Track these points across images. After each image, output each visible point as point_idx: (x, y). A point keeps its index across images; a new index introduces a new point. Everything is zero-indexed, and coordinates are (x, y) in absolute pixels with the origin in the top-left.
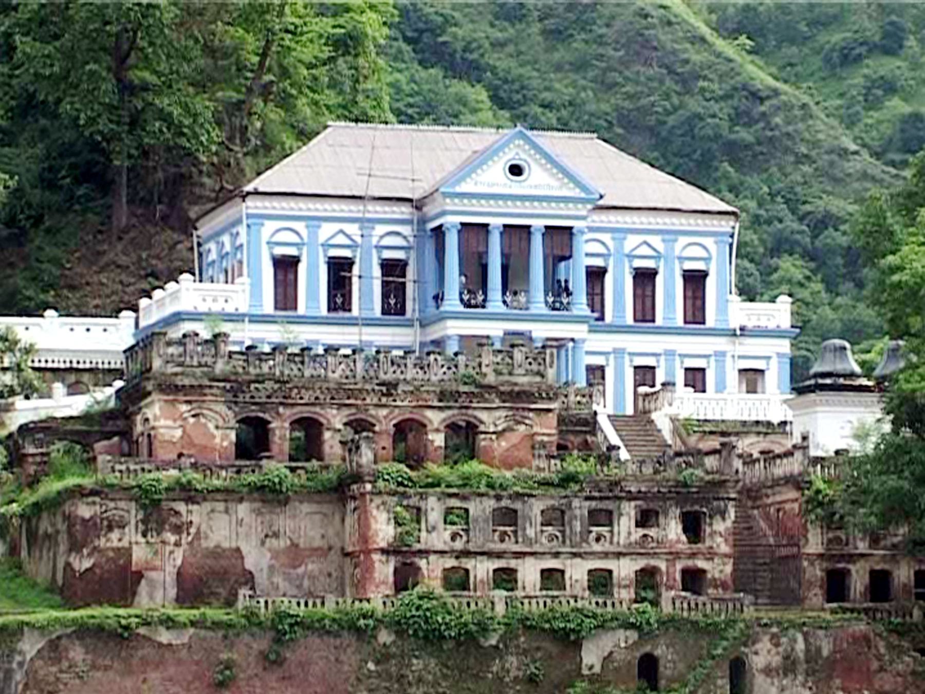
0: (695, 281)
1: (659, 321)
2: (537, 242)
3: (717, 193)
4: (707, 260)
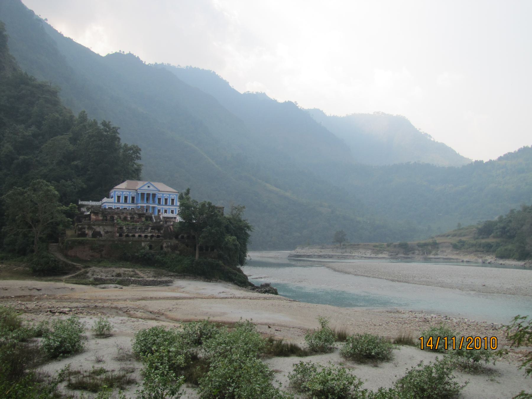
0: (173, 200)
2: (151, 195)
3: (175, 189)
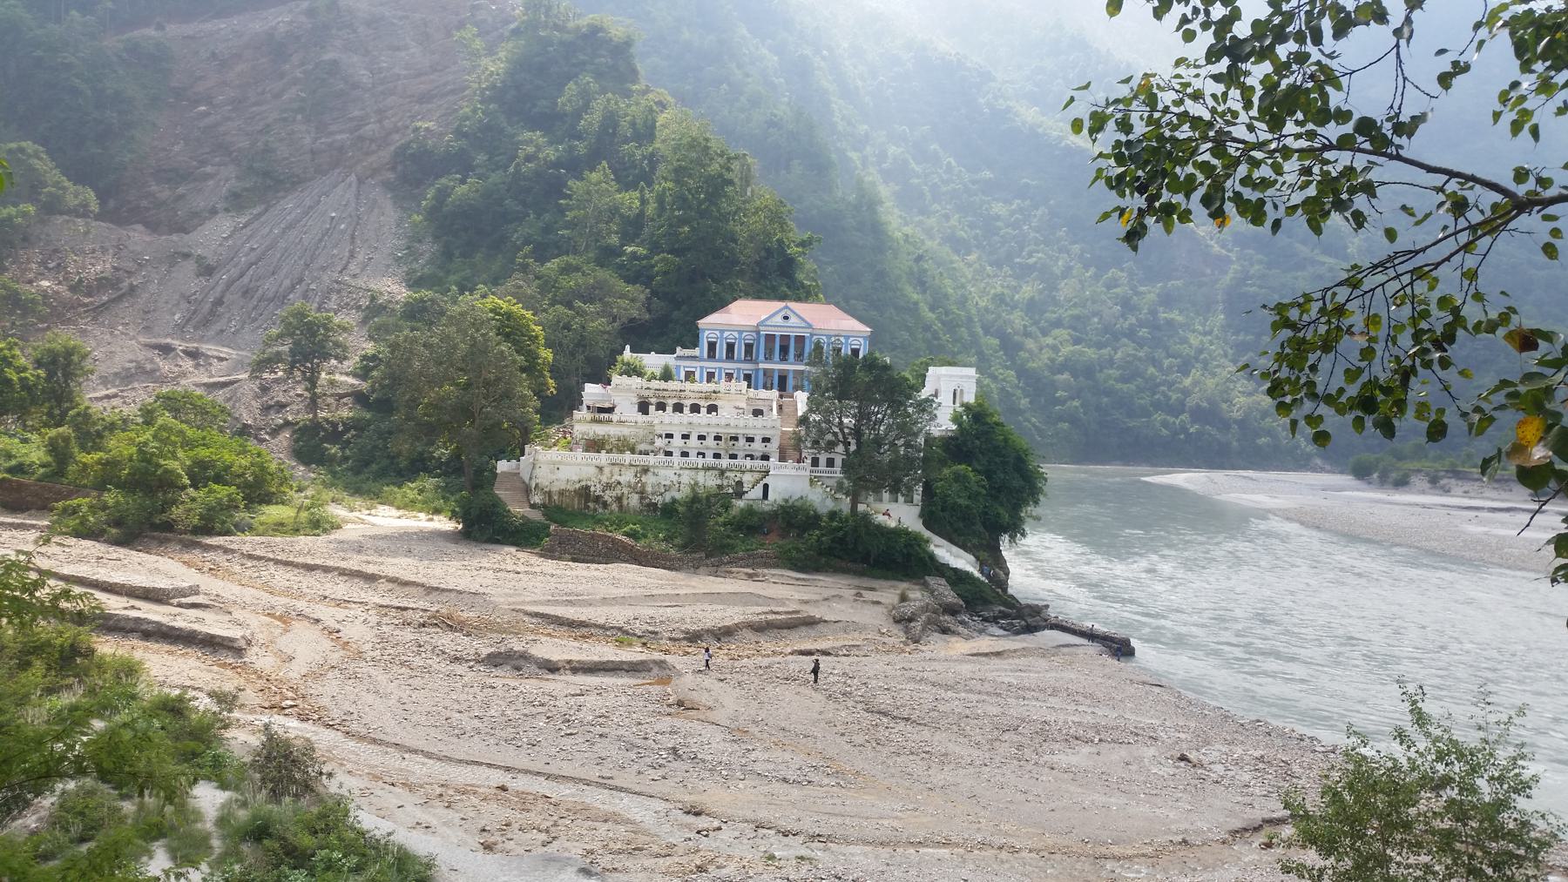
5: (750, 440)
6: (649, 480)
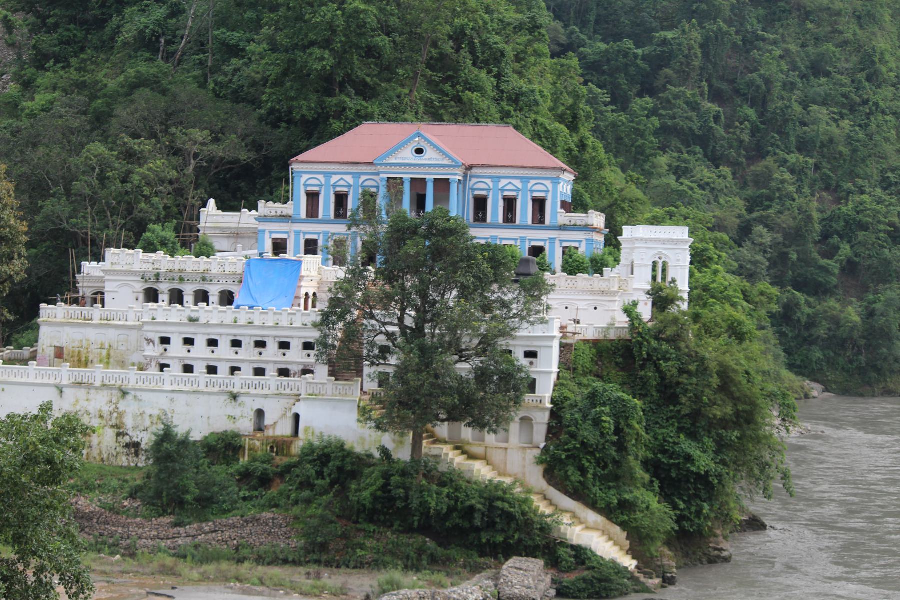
1: (518, 222)
4: (547, 192)
5: (285, 345)
6: (129, 407)
